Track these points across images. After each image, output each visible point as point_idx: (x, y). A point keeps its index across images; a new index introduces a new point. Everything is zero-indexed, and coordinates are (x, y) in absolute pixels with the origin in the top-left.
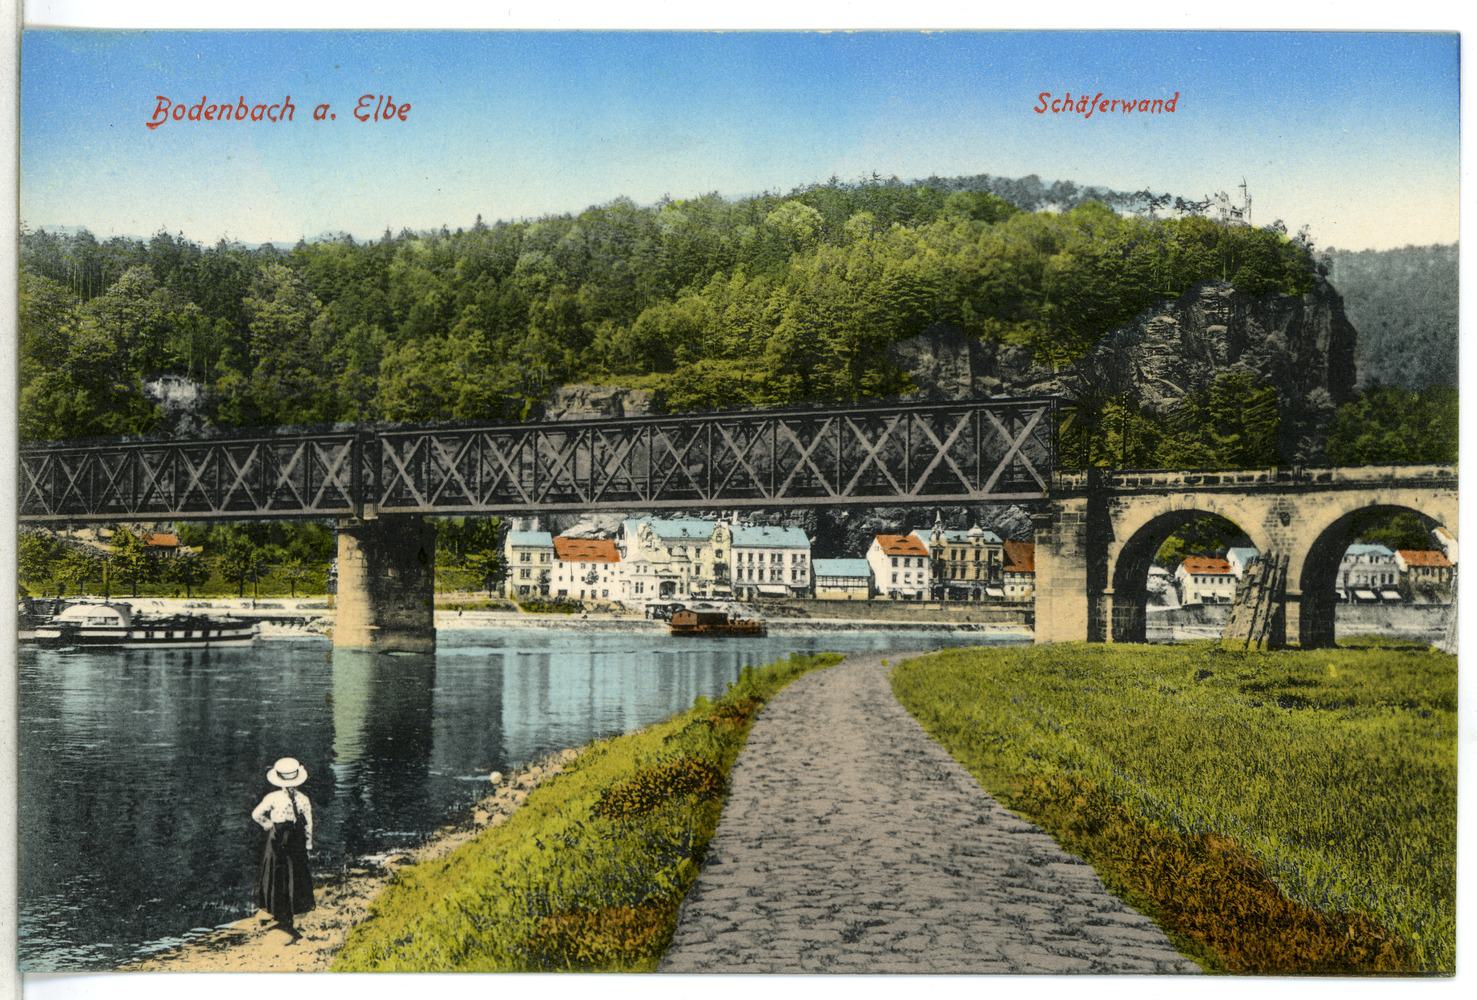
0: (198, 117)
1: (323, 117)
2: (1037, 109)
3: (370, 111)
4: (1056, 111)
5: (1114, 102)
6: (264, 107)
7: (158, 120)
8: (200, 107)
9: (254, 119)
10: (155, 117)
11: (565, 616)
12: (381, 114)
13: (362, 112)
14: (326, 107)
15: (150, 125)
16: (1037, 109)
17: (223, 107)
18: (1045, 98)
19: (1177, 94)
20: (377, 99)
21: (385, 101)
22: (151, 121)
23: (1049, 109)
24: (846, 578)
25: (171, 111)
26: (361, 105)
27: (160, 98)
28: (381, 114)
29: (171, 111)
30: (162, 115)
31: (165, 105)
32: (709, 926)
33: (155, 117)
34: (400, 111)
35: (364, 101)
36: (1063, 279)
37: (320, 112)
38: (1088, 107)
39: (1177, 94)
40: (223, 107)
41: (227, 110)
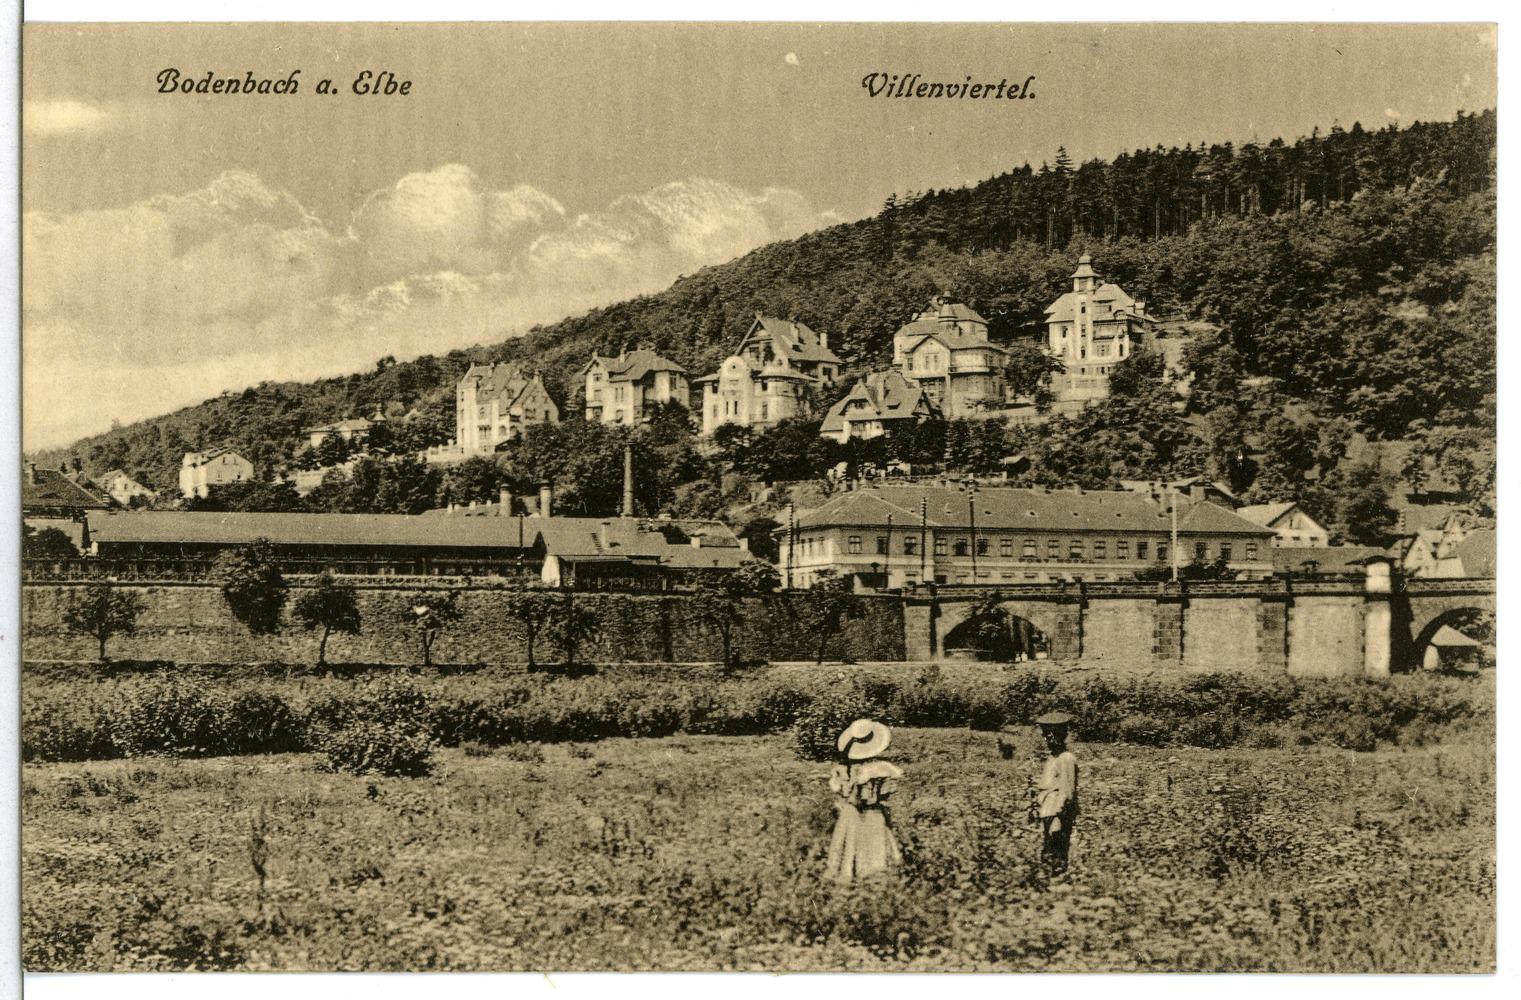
0: (267, 91)
8: (208, 81)
14: (328, 83)
37: (323, 88)
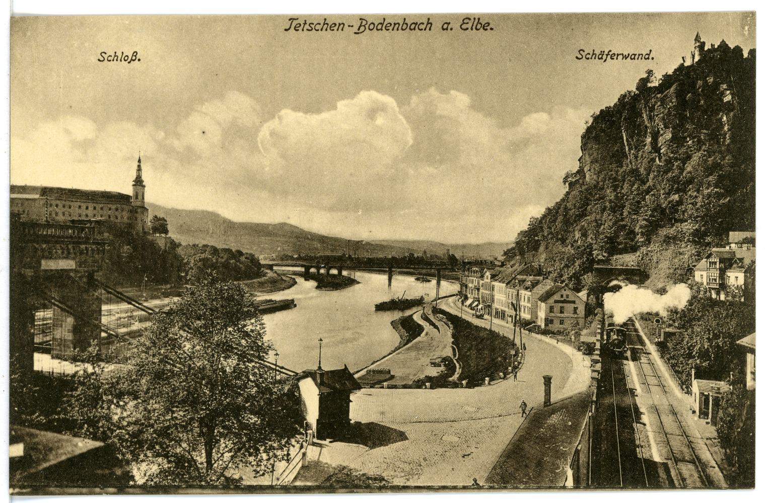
0: (382, 29)
1: (447, 29)
2: (99, 60)
3: (469, 26)
4: (588, 59)
5: (618, 55)
6: (416, 24)
7: (361, 31)
9: (377, 30)
10: (359, 29)
11: (374, 256)
12: (474, 27)
13: (464, 26)
15: (355, 33)
16: (99, 60)
17: (395, 24)
18: (310, 28)
19: (651, 51)
20: (473, 20)
21: (477, 21)
22: (357, 31)
23: (584, 58)
24: (282, 368)
25: (367, 26)
26: (464, 23)
27: (361, 19)
28: (474, 27)
29: (367, 26)
30: (362, 29)
31: (364, 23)
32: (707, 181)
33: (359, 29)
36: (516, 355)
37: (445, 26)
38: (604, 57)
39: (651, 51)
40: (340, 24)
41: (397, 26)
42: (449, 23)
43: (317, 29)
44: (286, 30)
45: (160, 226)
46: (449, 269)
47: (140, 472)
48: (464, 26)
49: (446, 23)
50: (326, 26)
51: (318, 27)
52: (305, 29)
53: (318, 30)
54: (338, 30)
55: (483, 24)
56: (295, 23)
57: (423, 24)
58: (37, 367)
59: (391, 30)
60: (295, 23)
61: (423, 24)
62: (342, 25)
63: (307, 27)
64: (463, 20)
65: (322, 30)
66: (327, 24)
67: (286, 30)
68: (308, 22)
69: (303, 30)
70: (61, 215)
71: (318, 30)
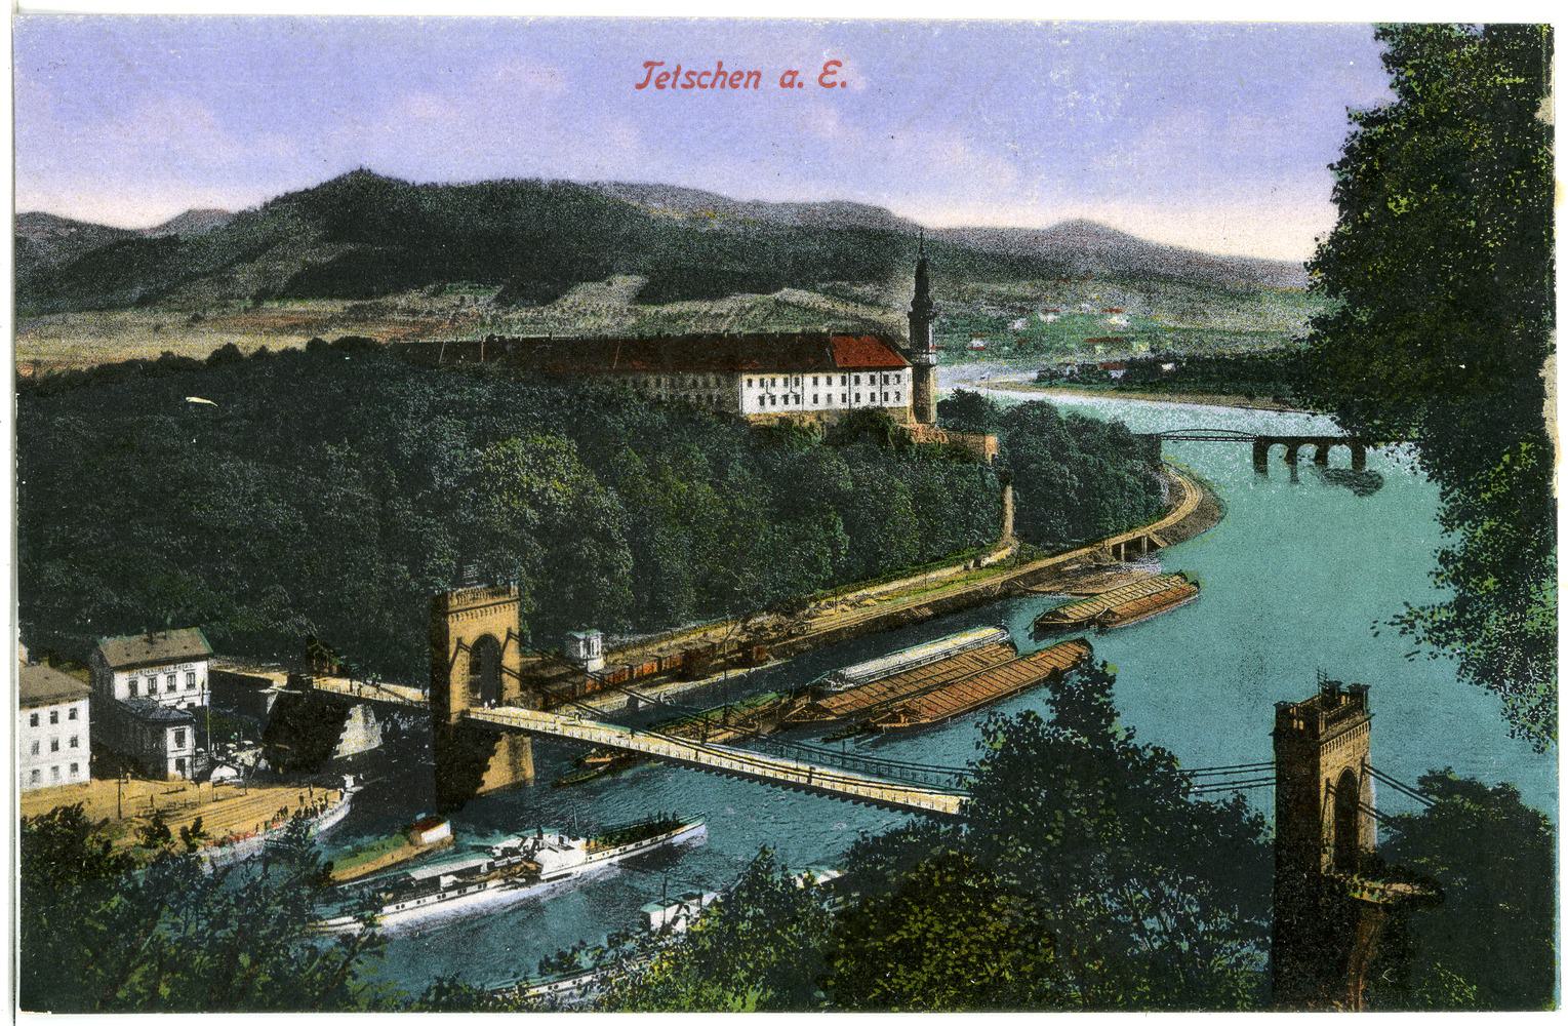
13: (828, 79)
18: (689, 83)
26: (826, 72)
34: (731, 79)
35: (831, 68)
37: (788, 79)
42: (796, 73)
43: (703, 82)
44: (640, 87)
45: (1254, 397)
46: (652, 596)
47: (1552, 712)
48: (828, 79)
49: (789, 72)
50: (721, 77)
51: (706, 80)
52: (678, 84)
53: (705, 86)
54: (746, 86)
55: (730, 75)
56: (657, 71)
57: (707, 73)
58: (168, 730)
59: (669, 88)
60: (657, 71)
61: (707, 73)
62: (754, 78)
63: (682, 78)
64: (825, 68)
65: (713, 85)
66: (725, 74)
67: (640, 87)
68: (684, 70)
69: (674, 86)
70: (780, 401)
71: (705, 86)
